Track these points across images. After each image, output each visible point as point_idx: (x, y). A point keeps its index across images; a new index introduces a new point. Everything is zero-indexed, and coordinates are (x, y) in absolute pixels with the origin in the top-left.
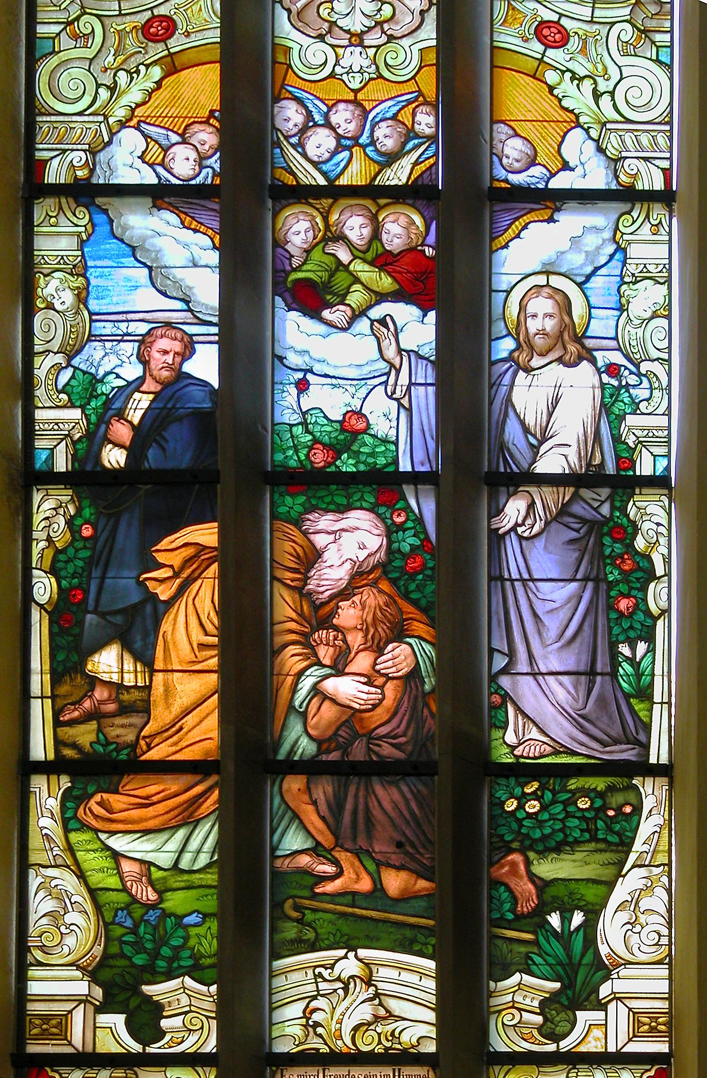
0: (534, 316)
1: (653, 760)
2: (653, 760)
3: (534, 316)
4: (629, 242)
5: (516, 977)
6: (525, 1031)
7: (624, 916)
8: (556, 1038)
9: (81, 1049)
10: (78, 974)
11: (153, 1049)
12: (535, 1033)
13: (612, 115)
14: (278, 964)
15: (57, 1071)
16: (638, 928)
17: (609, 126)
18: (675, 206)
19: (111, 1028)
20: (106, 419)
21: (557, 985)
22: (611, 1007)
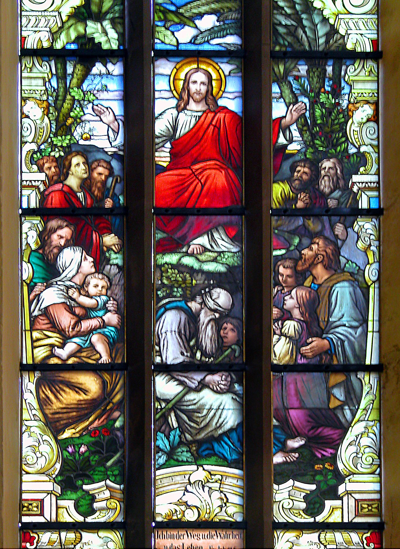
0: (195, 82)
1: (368, 362)
2: (368, 362)
3: (195, 82)
4: (353, 81)
5: (291, 482)
6: (295, 511)
7: (353, 449)
8: (313, 515)
9: (49, 520)
10: (47, 479)
11: (89, 519)
12: (302, 513)
13: (342, 10)
14: (376, 496)
15: (36, 533)
16: (360, 456)
17: (340, 16)
18: (380, 61)
19: (66, 509)
20: (333, 238)
21: (313, 487)
22: (345, 499)
